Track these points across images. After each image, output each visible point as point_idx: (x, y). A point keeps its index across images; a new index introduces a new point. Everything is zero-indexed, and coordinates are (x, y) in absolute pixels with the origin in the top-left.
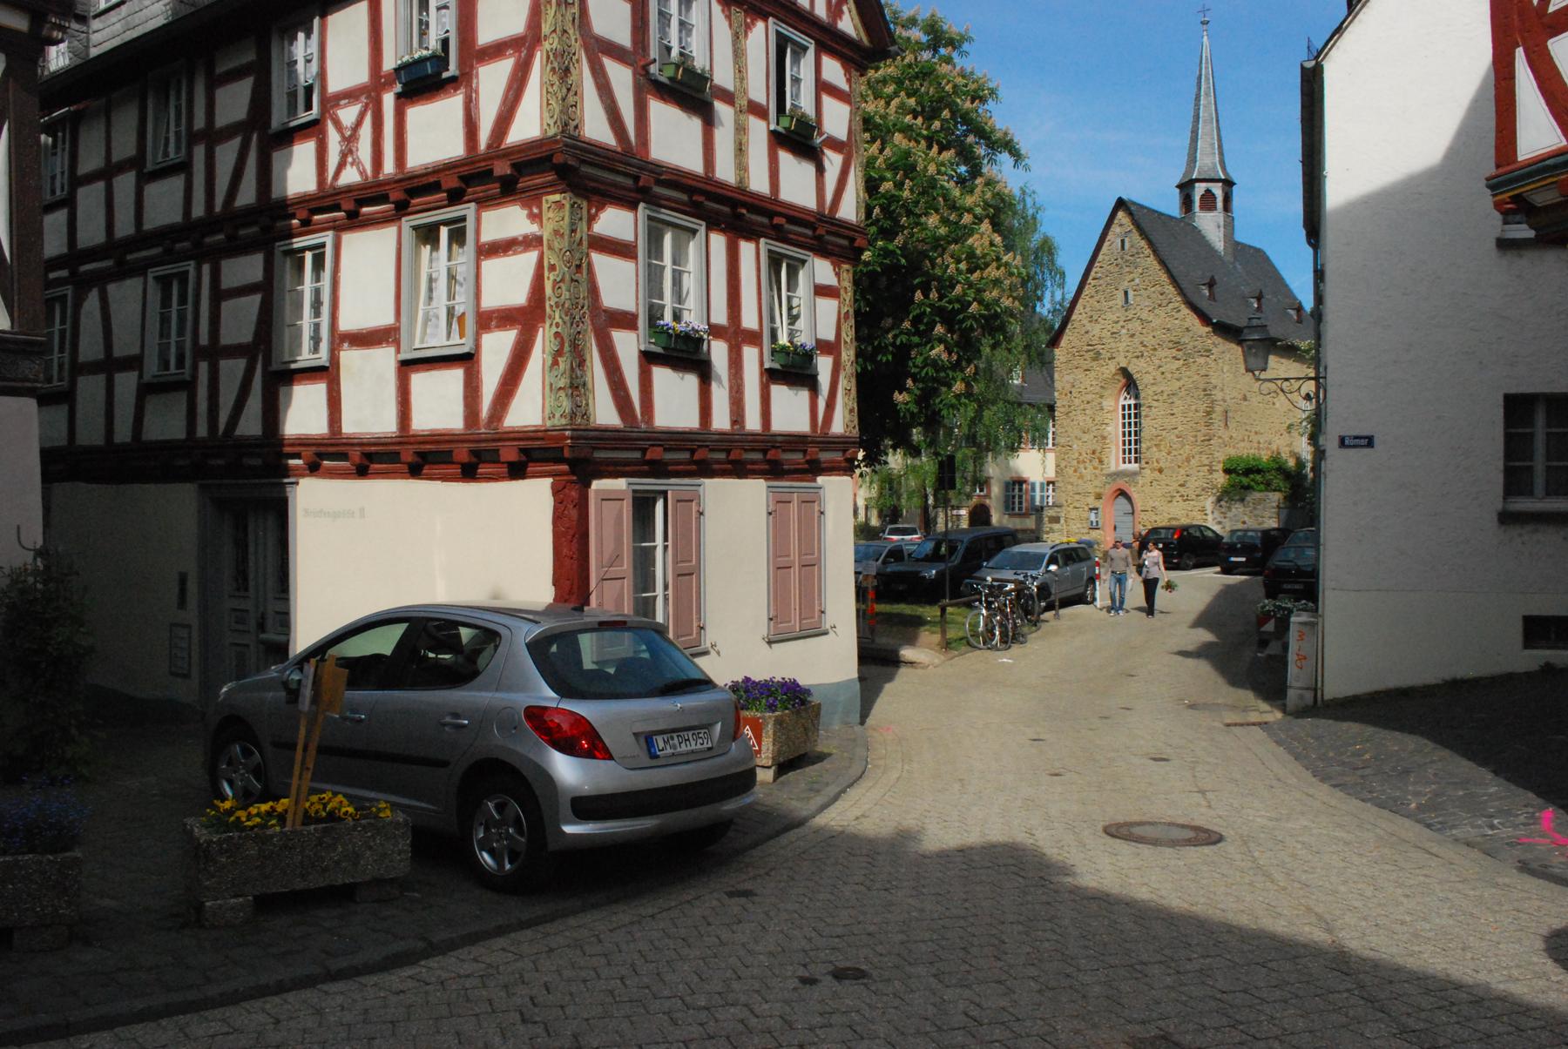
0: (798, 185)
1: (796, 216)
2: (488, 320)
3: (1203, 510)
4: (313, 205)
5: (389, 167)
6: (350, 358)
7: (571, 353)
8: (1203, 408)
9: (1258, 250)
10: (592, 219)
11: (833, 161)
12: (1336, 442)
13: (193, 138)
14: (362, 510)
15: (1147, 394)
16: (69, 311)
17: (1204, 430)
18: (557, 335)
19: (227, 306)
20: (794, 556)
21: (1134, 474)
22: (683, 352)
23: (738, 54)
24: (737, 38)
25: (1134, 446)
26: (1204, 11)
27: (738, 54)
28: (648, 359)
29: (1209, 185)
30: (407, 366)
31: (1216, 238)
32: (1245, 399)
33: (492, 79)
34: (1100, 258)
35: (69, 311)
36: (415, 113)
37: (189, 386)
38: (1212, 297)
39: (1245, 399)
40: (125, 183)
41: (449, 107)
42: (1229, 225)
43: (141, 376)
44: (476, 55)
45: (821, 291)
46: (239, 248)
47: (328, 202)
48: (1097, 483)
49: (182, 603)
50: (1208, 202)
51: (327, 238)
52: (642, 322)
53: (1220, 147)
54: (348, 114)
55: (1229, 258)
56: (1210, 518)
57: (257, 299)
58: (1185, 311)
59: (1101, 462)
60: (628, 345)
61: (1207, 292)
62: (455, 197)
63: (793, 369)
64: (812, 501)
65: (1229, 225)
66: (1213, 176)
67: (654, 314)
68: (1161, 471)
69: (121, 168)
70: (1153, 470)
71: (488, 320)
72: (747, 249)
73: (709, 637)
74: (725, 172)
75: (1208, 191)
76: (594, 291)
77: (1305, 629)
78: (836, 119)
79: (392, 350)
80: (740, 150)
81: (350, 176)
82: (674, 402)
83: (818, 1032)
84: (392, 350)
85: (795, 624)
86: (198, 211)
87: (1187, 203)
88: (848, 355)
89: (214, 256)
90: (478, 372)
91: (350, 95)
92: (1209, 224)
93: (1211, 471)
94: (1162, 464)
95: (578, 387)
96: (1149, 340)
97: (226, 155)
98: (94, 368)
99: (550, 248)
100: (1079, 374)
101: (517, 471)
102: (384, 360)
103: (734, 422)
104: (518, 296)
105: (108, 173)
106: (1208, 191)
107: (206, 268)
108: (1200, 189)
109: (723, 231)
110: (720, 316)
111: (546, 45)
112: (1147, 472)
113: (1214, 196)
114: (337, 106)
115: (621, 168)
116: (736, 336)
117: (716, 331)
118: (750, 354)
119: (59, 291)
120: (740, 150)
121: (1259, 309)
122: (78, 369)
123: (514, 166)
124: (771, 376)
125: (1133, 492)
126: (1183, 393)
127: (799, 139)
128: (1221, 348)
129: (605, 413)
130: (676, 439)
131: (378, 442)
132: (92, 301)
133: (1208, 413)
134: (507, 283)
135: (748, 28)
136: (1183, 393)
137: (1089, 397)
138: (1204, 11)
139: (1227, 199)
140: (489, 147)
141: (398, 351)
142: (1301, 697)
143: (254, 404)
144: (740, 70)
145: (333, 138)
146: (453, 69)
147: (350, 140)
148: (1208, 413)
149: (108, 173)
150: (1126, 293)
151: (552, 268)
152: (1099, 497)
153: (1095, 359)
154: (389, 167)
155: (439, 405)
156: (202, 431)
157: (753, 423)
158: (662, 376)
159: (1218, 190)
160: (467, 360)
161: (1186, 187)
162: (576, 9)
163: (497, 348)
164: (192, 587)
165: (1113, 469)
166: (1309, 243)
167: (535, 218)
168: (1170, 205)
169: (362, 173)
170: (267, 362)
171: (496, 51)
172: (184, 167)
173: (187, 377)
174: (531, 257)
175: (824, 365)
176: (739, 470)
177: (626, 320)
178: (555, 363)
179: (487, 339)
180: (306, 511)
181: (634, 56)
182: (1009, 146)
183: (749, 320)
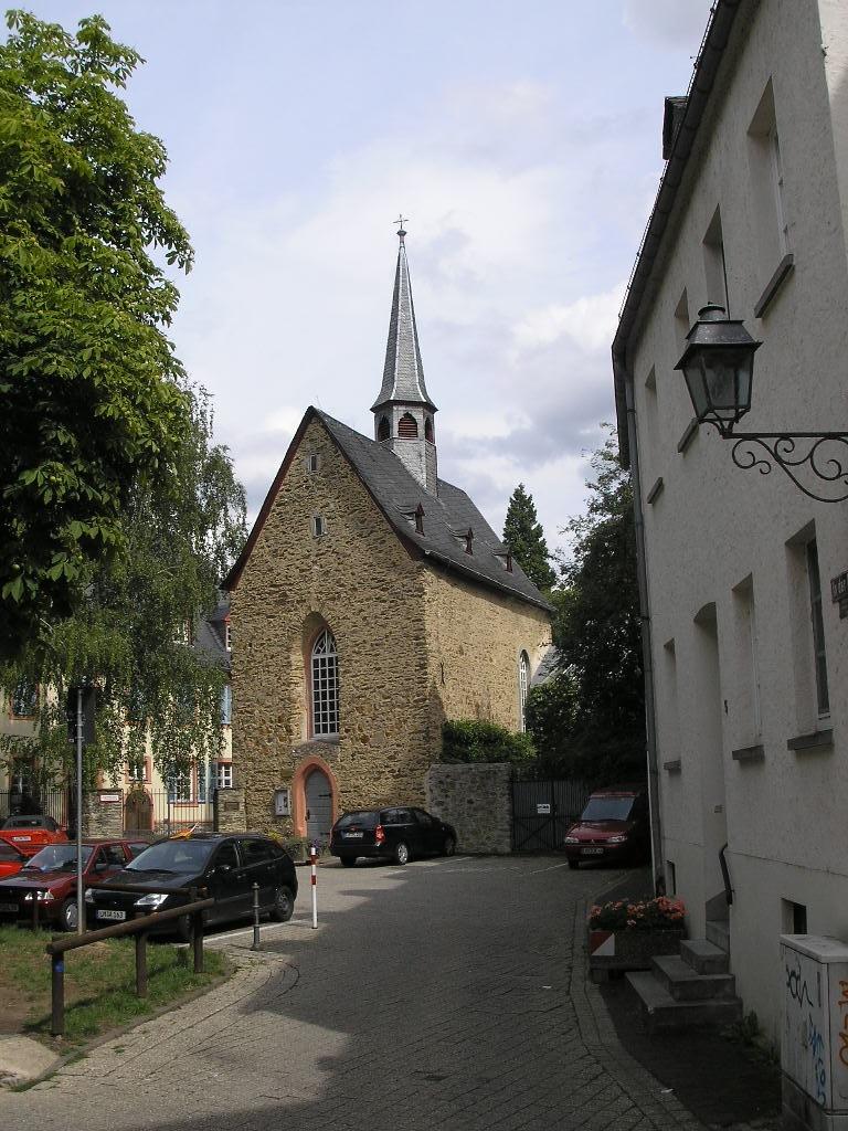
3: (419, 788)
15: (346, 646)
16: (207, 778)
17: (417, 688)
25: (327, 715)
29: (409, 409)
32: (461, 652)
34: (287, 479)
35: (207, 778)
38: (420, 528)
39: (461, 652)
55: (432, 493)
56: (428, 798)
58: (393, 540)
59: (290, 731)
61: (413, 523)
66: (413, 399)
68: (365, 740)
75: (407, 415)
87: (383, 428)
92: (407, 451)
93: (428, 738)
96: (349, 580)
100: (262, 622)
106: (407, 415)
108: (398, 414)
121: (469, 550)
128: (435, 587)
137: (275, 650)
139: (429, 426)
150: (318, 521)
152: (286, 777)
153: (282, 602)
159: (419, 416)
161: (382, 410)
164: (723, 708)
168: (367, 427)
182: (173, 236)
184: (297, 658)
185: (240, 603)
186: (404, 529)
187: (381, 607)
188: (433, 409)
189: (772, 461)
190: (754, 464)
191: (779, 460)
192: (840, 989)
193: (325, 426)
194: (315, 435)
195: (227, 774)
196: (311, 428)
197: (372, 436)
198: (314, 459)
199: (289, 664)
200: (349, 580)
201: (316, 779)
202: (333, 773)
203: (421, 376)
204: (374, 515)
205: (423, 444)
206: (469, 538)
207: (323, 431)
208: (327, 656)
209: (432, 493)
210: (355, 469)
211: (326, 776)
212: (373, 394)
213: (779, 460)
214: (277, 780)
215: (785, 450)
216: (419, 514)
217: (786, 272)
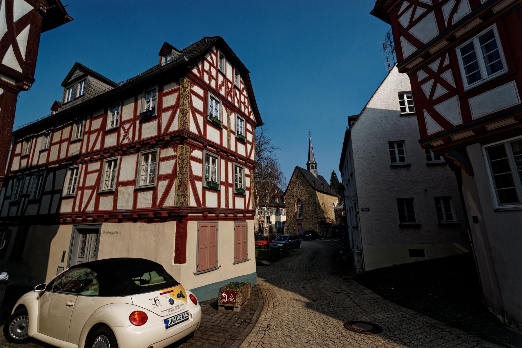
0: (241, 150)
1: (241, 157)
2: (162, 178)
4: (115, 149)
5: (136, 139)
6: (121, 189)
7: (182, 186)
9: (339, 168)
10: (191, 152)
11: (249, 146)
13: (85, 133)
14: (120, 231)
18: (180, 181)
19: (88, 176)
20: (241, 241)
21: (302, 219)
22: (213, 187)
23: (229, 119)
24: (229, 115)
26: (310, 133)
27: (229, 119)
28: (204, 189)
30: (137, 191)
31: (315, 175)
33: (166, 117)
36: (145, 126)
37: (75, 198)
40: (65, 145)
41: (154, 124)
42: (317, 171)
43: (61, 195)
44: (162, 110)
45: (247, 176)
46: (93, 161)
47: (119, 148)
49: (63, 260)
50: (312, 167)
51: (119, 158)
52: (204, 179)
54: (127, 126)
57: (97, 174)
58: (310, 187)
60: (199, 185)
62: (153, 146)
63: (239, 193)
64: (216, 230)
65: (317, 173)
67: (207, 179)
69: (64, 141)
71: (162, 178)
72: (230, 164)
73: (219, 264)
74: (225, 145)
76: (191, 170)
78: (250, 137)
79: (133, 186)
80: (229, 140)
81: (126, 141)
82: (211, 200)
83: (228, 324)
84: (133, 186)
85: (241, 259)
86: (84, 151)
88: (252, 191)
89: (87, 163)
90: (157, 192)
91: (128, 121)
92: (312, 171)
95: (185, 196)
97: (93, 137)
98: (48, 193)
99: (179, 158)
100: (290, 200)
101: (164, 220)
102: (131, 189)
103: (226, 206)
104: (170, 171)
105: (60, 142)
107: (84, 166)
108: (311, 165)
109: (224, 159)
110: (223, 179)
111: (181, 108)
114: (124, 124)
115: (199, 140)
116: (227, 184)
117: (222, 183)
118: (230, 189)
119: (42, 173)
120: (229, 140)
122: (44, 193)
123: (170, 138)
124: (235, 195)
127: (241, 140)
129: (192, 203)
130: (212, 210)
131: (127, 211)
132: (51, 175)
134: (166, 168)
135: (231, 114)
138: (310, 133)
140: (164, 133)
141: (135, 187)
143: (93, 202)
144: (229, 123)
145: (122, 132)
146: (156, 114)
147: (127, 132)
149: (60, 142)
151: (179, 164)
152: (295, 225)
154: (136, 139)
155: (145, 201)
156: (76, 210)
157: (231, 206)
158: (208, 194)
159: (314, 165)
160: (154, 189)
161: (308, 164)
162: (189, 100)
163: (163, 185)
166: (335, 174)
167: (175, 151)
168: (306, 168)
169: (129, 140)
170: (98, 190)
171: (167, 109)
172: (81, 140)
173: (74, 195)
174: (174, 161)
175: (247, 193)
176: (226, 218)
177: (199, 179)
178: (179, 189)
179: (160, 183)
180: (104, 232)
181: (204, 114)
183: (230, 181)
184: (296, 206)
216: (314, 182)
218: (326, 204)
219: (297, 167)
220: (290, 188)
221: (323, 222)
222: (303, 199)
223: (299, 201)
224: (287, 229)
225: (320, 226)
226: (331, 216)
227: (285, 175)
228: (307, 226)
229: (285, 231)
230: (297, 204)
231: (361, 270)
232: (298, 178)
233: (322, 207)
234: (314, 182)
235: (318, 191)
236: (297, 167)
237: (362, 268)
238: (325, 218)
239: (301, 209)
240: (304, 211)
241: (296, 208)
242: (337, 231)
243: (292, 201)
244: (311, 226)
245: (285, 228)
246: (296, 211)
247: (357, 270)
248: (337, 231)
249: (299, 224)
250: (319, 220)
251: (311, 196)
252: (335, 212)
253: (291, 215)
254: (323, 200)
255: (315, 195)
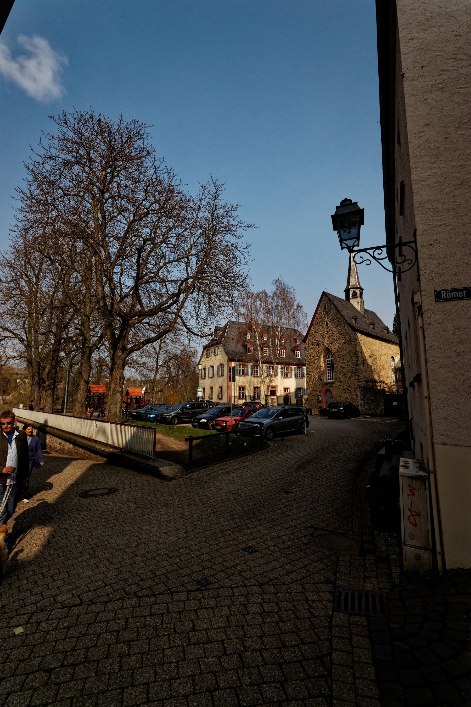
3: (357, 395)
8: (354, 359)
9: (373, 313)
12: (432, 298)
17: (355, 367)
21: (333, 383)
31: (359, 308)
38: (356, 322)
42: (362, 303)
48: (320, 387)
50: (355, 295)
53: (358, 278)
55: (363, 313)
58: (347, 326)
61: (354, 321)
65: (362, 306)
66: (356, 287)
68: (341, 382)
70: (339, 382)
75: (354, 292)
77: (417, 484)
92: (355, 302)
93: (359, 382)
94: (341, 380)
96: (335, 338)
100: (313, 350)
106: (354, 292)
108: (351, 291)
112: (337, 382)
113: (356, 293)
121: (374, 328)
125: (332, 390)
126: (348, 355)
133: (357, 361)
136: (348, 355)
137: (316, 358)
142: (418, 557)
148: (357, 361)
150: (327, 323)
153: (318, 345)
159: (358, 292)
161: (347, 291)
165: (325, 382)
168: (342, 296)
184: (322, 360)
185: (307, 346)
186: (351, 323)
187: (345, 345)
188: (363, 289)
189: (371, 259)
190: (363, 262)
191: (374, 258)
192: (408, 488)
193: (328, 297)
194: (325, 299)
195: (300, 391)
196: (324, 297)
197: (344, 299)
198: (325, 306)
199: (320, 362)
200: (335, 338)
201: (328, 393)
202: (333, 391)
203: (358, 280)
204: (341, 320)
205: (359, 299)
206: (373, 324)
207: (327, 298)
208: (331, 359)
209: (363, 313)
210: (336, 307)
211: (331, 392)
212: (344, 286)
213: (374, 258)
214: (318, 393)
215: (378, 254)
216: (356, 319)
217: (393, 357)
218: (377, 357)
219: (324, 294)
220: (312, 331)
221: (371, 388)
222: (334, 348)
223: (328, 351)
224: (307, 400)
225: (364, 395)
226: (387, 377)
227: (304, 309)
228: (341, 394)
229: (304, 402)
230: (325, 358)
231: (425, 555)
232: (327, 312)
233: (370, 361)
234: (356, 319)
235: (363, 333)
236: (324, 294)
237: (432, 548)
238: (375, 382)
239: (330, 365)
240: (336, 369)
241: (322, 364)
242: (395, 403)
243: (316, 353)
244: (348, 395)
245: (305, 397)
246: (322, 368)
247: (409, 552)
248: (395, 403)
249: (328, 390)
250: (362, 384)
251: (348, 342)
252: (395, 373)
253: (315, 375)
254: (371, 349)
255: (356, 339)
